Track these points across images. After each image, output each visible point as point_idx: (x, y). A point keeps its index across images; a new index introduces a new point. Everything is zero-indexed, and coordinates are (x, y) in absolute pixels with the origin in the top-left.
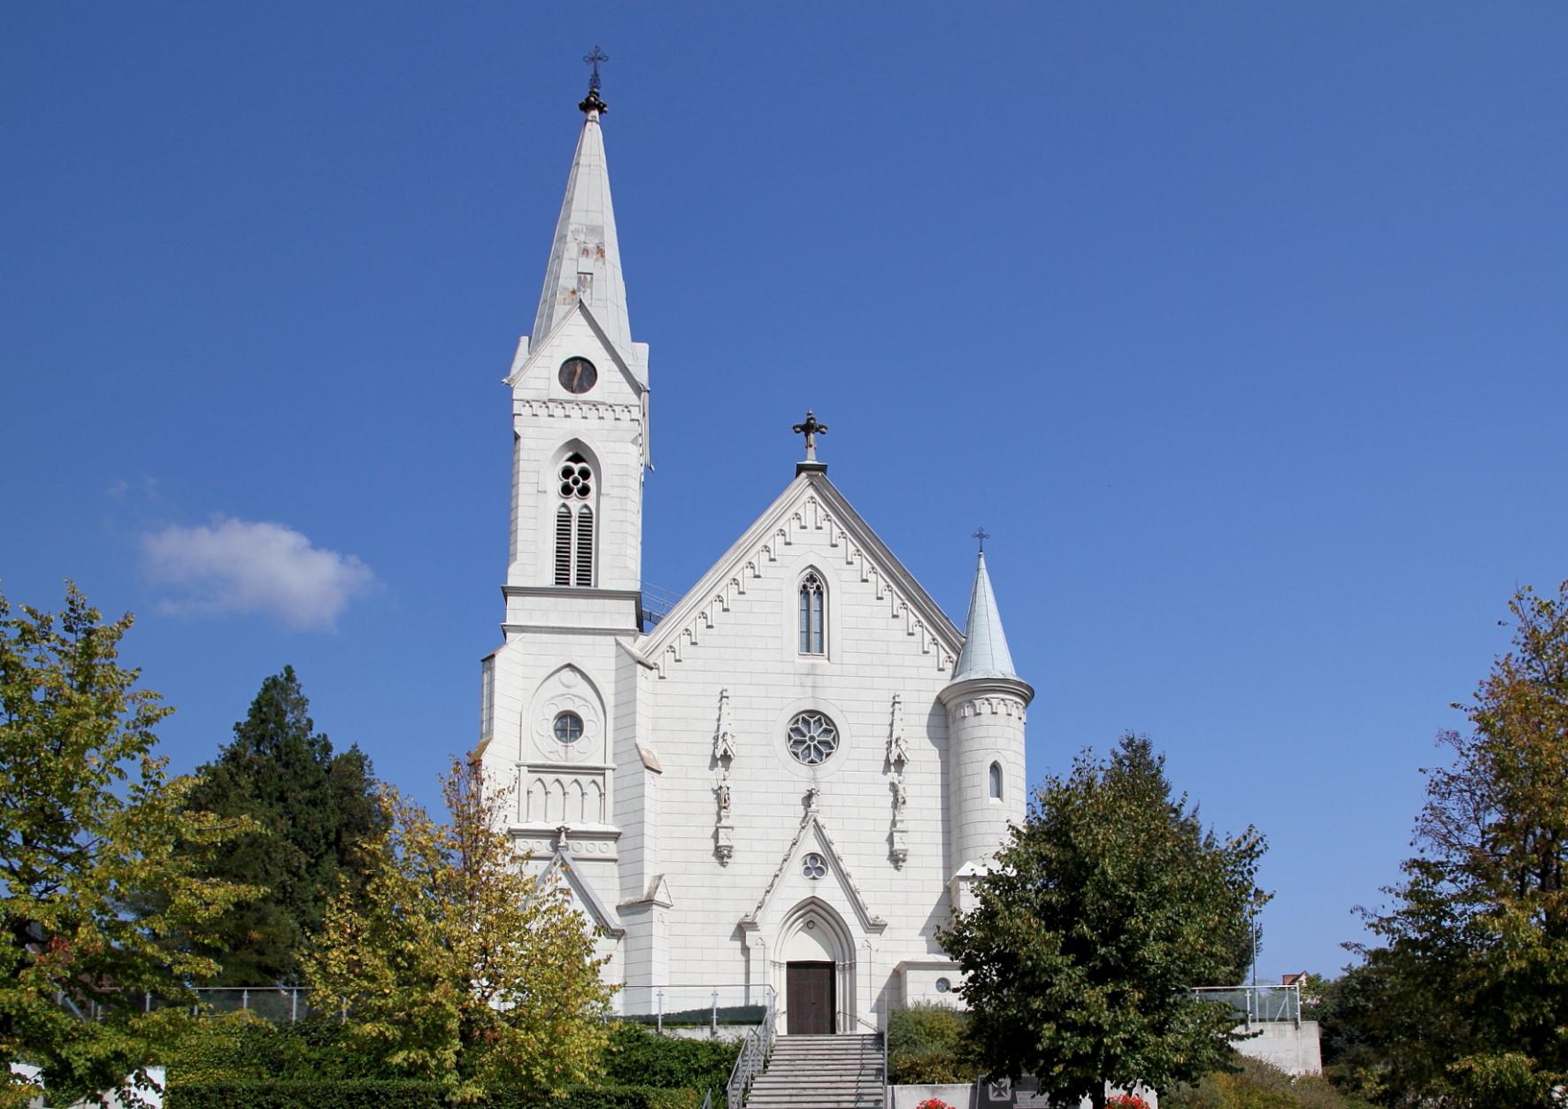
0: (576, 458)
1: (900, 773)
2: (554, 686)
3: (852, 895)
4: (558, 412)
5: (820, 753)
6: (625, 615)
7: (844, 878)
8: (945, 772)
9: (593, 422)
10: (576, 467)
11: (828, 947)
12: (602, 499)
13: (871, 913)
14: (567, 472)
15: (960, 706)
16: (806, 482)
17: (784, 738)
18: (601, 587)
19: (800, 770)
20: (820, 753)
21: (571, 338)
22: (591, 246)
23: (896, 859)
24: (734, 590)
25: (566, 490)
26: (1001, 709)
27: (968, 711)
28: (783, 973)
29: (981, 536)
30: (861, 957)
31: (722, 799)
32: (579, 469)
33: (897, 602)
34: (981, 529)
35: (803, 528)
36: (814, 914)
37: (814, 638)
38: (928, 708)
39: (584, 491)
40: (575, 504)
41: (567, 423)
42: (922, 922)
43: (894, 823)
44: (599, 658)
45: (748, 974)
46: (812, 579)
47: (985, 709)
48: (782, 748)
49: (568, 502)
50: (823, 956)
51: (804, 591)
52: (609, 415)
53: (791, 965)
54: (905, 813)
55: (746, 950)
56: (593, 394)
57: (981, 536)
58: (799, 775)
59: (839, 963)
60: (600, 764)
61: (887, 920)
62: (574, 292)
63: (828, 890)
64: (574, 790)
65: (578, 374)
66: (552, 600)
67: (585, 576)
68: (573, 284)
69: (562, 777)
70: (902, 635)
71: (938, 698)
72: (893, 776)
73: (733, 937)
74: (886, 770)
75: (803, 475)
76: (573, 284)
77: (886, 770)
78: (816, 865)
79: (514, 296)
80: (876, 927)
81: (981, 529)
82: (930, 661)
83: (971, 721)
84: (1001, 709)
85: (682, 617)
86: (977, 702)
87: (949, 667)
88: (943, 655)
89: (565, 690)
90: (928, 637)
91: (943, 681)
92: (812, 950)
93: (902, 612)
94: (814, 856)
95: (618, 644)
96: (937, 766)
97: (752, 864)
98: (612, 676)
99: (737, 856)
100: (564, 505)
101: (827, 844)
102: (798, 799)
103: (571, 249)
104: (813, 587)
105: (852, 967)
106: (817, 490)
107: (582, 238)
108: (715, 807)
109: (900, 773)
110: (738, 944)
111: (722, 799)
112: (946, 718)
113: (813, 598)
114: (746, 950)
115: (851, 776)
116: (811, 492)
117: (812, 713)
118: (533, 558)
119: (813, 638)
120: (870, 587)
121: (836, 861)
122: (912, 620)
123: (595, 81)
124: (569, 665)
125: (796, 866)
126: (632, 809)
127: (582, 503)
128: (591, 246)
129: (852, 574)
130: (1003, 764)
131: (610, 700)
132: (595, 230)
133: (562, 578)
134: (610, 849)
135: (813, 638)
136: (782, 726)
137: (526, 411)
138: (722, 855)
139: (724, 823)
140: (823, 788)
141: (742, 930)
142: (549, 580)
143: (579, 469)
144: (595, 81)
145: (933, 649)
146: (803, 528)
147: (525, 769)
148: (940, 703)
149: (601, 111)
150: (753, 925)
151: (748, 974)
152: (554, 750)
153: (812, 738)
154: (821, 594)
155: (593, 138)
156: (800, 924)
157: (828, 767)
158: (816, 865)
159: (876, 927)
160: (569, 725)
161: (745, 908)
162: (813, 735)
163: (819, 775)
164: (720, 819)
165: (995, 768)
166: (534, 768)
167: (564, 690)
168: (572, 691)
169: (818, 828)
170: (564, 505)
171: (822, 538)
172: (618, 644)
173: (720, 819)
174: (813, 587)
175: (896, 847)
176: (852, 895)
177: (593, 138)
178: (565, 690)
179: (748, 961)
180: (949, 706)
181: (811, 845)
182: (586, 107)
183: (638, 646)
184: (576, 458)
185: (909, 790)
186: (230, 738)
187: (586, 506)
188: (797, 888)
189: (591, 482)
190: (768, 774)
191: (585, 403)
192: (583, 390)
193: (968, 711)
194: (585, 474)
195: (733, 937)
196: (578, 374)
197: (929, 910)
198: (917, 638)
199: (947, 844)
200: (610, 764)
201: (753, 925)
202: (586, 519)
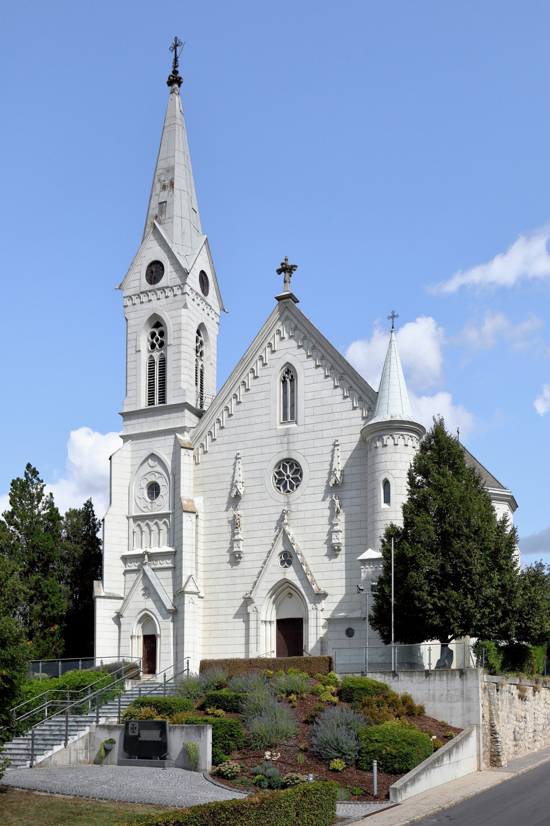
2: (146, 468)
4: (144, 299)
14: (153, 335)
19: (280, 497)
22: (167, 182)
25: (153, 346)
26: (401, 442)
34: (393, 312)
41: (150, 305)
47: (390, 442)
51: (284, 382)
56: (163, 283)
61: (328, 591)
64: (154, 528)
67: (163, 399)
78: (288, 558)
83: (380, 450)
86: (385, 438)
97: (250, 562)
99: (245, 557)
104: (289, 375)
107: (163, 178)
111: (235, 524)
119: (290, 412)
125: (276, 560)
126: (175, 537)
130: (391, 480)
134: (167, 563)
135: (290, 412)
142: (143, 404)
147: (131, 520)
152: (148, 507)
162: (288, 474)
165: (386, 483)
167: (150, 469)
174: (289, 375)
186: (94, 509)
188: (276, 572)
190: (263, 501)
191: (159, 289)
193: (379, 444)
195: (237, 616)
202: (163, 362)
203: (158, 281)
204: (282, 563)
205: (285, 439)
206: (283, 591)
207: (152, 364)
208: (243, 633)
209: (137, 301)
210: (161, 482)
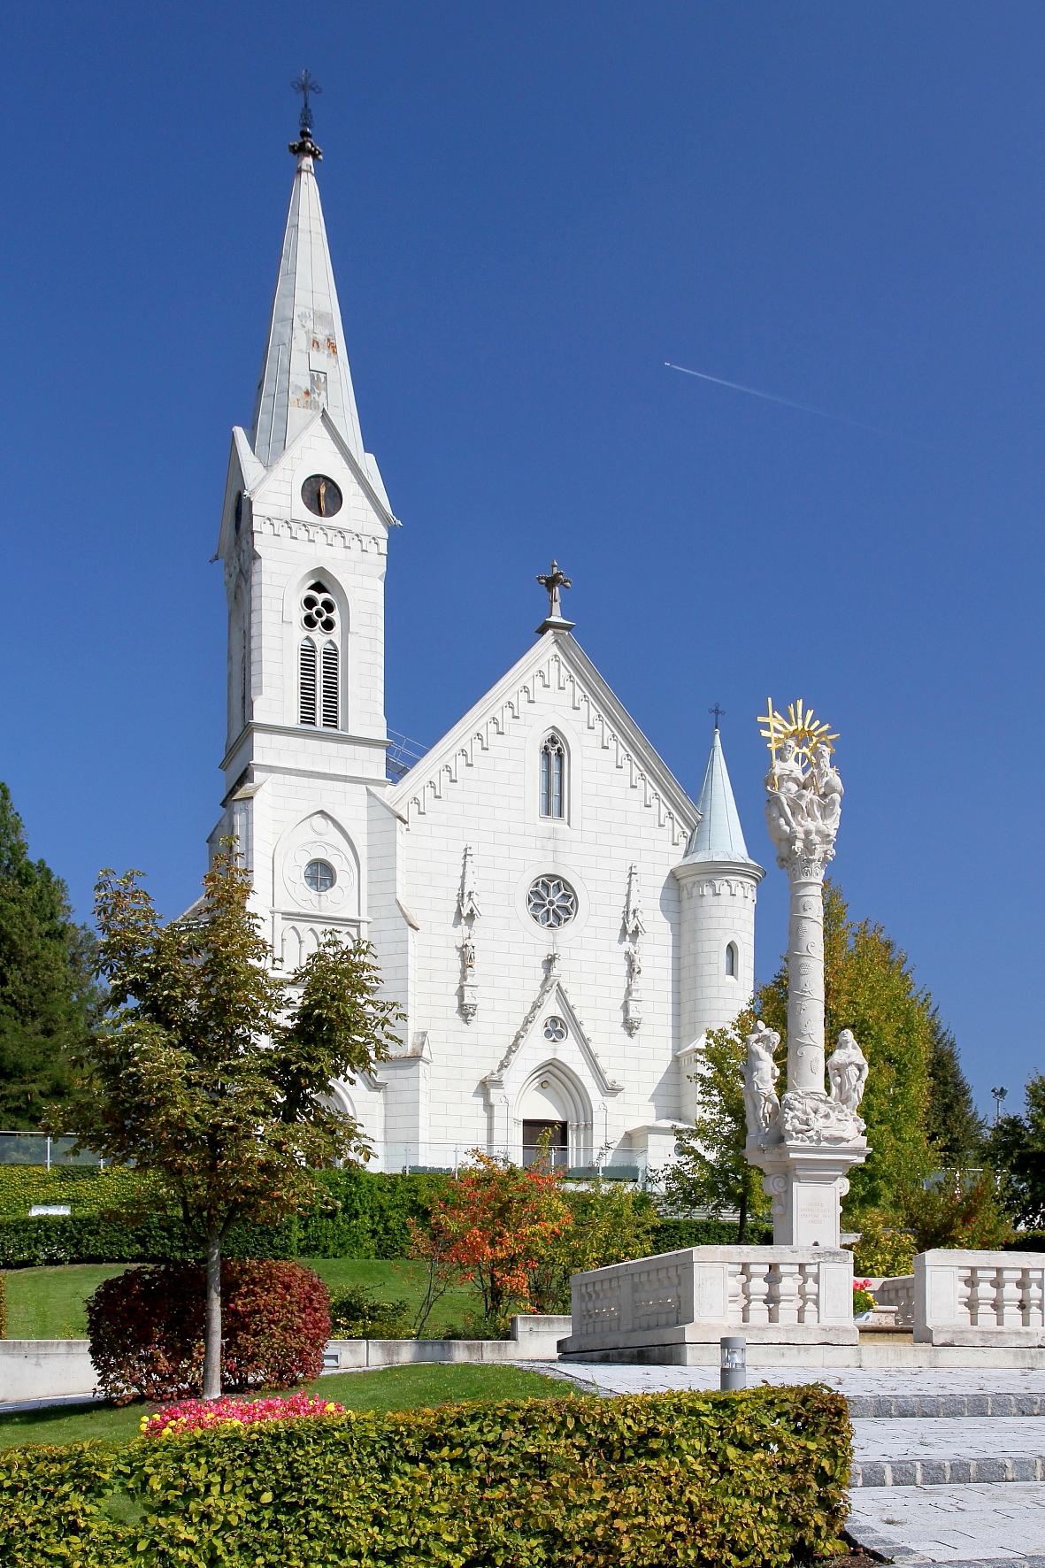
0: (318, 587)
1: (470, 927)
3: (592, 1060)
5: (558, 918)
6: (374, 763)
7: (584, 1042)
8: (677, 946)
9: (338, 551)
10: (321, 597)
11: (561, 1107)
12: (351, 638)
13: (609, 1077)
14: (310, 602)
15: (698, 884)
16: (552, 639)
17: (524, 900)
18: (352, 732)
19: (540, 932)
20: (558, 918)
21: (312, 452)
23: (630, 1026)
24: (477, 744)
25: (310, 622)
26: (739, 892)
27: (707, 890)
28: (520, 1130)
29: (717, 712)
30: (598, 1118)
31: (466, 957)
32: (321, 603)
33: (636, 773)
34: (723, 713)
35: (545, 689)
36: (552, 1075)
37: (554, 801)
38: (662, 881)
39: (328, 625)
40: (320, 638)
42: (652, 1089)
43: (629, 992)
44: (351, 807)
45: (490, 1130)
46: (553, 741)
47: (725, 890)
48: (524, 910)
49: (312, 635)
50: (554, 1115)
51: (546, 753)
52: (355, 544)
53: (526, 1123)
54: (640, 982)
55: (489, 1107)
56: (338, 520)
57: (717, 712)
58: (539, 938)
59: (572, 1124)
60: (355, 917)
61: (623, 1084)
62: (307, 393)
63: (568, 1052)
65: (322, 495)
66: (300, 740)
67: (331, 719)
68: (307, 384)
69: (299, 925)
70: (639, 806)
71: (672, 872)
72: (627, 945)
73: (476, 1094)
74: (622, 939)
75: (550, 632)
76: (307, 384)
77: (622, 939)
78: (555, 1029)
79: (237, 383)
80: (611, 1090)
81: (723, 713)
82: (665, 834)
84: (739, 892)
85: (428, 767)
86: (717, 883)
87: (683, 842)
88: (678, 830)
89: (317, 838)
90: (664, 811)
91: (676, 859)
92: (547, 1111)
93: (640, 783)
94: (554, 1019)
95: (369, 793)
96: (669, 939)
98: (364, 827)
100: (308, 638)
101: (569, 1009)
102: (538, 962)
103: (300, 341)
104: (554, 751)
105: (588, 1127)
106: (561, 648)
108: (459, 965)
109: (470, 927)
110: (480, 1101)
111: (466, 957)
112: (681, 891)
113: (553, 758)
114: (489, 1107)
115: (588, 945)
116: (555, 649)
117: (552, 877)
118: (276, 695)
119: (554, 801)
120: (610, 754)
121: (577, 1025)
122: (650, 791)
123: (306, 118)
124: (321, 812)
127: (328, 638)
128: (321, 338)
129: (592, 739)
131: (363, 852)
132: (320, 317)
133: (308, 718)
135: (554, 801)
136: (525, 887)
137: (267, 529)
138: (465, 1012)
139: (469, 981)
140: (562, 952)
141: (484, 1087)
143: (321, 603)
144: (306, 118)
145: (668, 822)
146: (545, 689)
147: (278, 917)
148: (673, 876)
149: (315, 156)
150: (498, 1083)
151: (490, 1130)
153: (551, 903)
154: (560, 755)
155: (308, 195)
156: (536, 1083)
157: (567, 930)
158: (555, 1029)
159: (611, 1090)
160: (321, 874)
161: (488, 1067)
162: (553, 900)
163: (558, 940)
164: (464, 978)
166: (288, 916)
168: (325, 839)
169: (561, 993)
170: (308, 638)
171: (565, 698)
172: (369, 793)
173: (464, 978)
174: (554, 751)
175: (631, 1015)
176: (592, 1060)
177: (308, 195)
178: (317, 838)
179: (491, 1118)
180: (683, 882)
181: (552, 1008)
182: (300, 150)
183: (388, 793)
184: (318, 587)
185: (642, 962)
187: (331, 642)
188: (537, 1049)
189: (335, 616)
190: (511, 939)
191: (330, 528)
192: (330, 514)
193: (707, 890)
194: (328, 606)
195: (476, 1094)
196: (322, 495)
197: (659, 1077)
198: (654, 810)
199: (677, 1015)
200: (364, 917)
201: (498, 1083)
202: (331, 655)
203: (109, 1285)
204: (548, 1034)
205: (550, 845)
206: (552, 1075)
207: (308, 653)
208: (484, 1123)
209: (285, 532)
210: (335, 862)
